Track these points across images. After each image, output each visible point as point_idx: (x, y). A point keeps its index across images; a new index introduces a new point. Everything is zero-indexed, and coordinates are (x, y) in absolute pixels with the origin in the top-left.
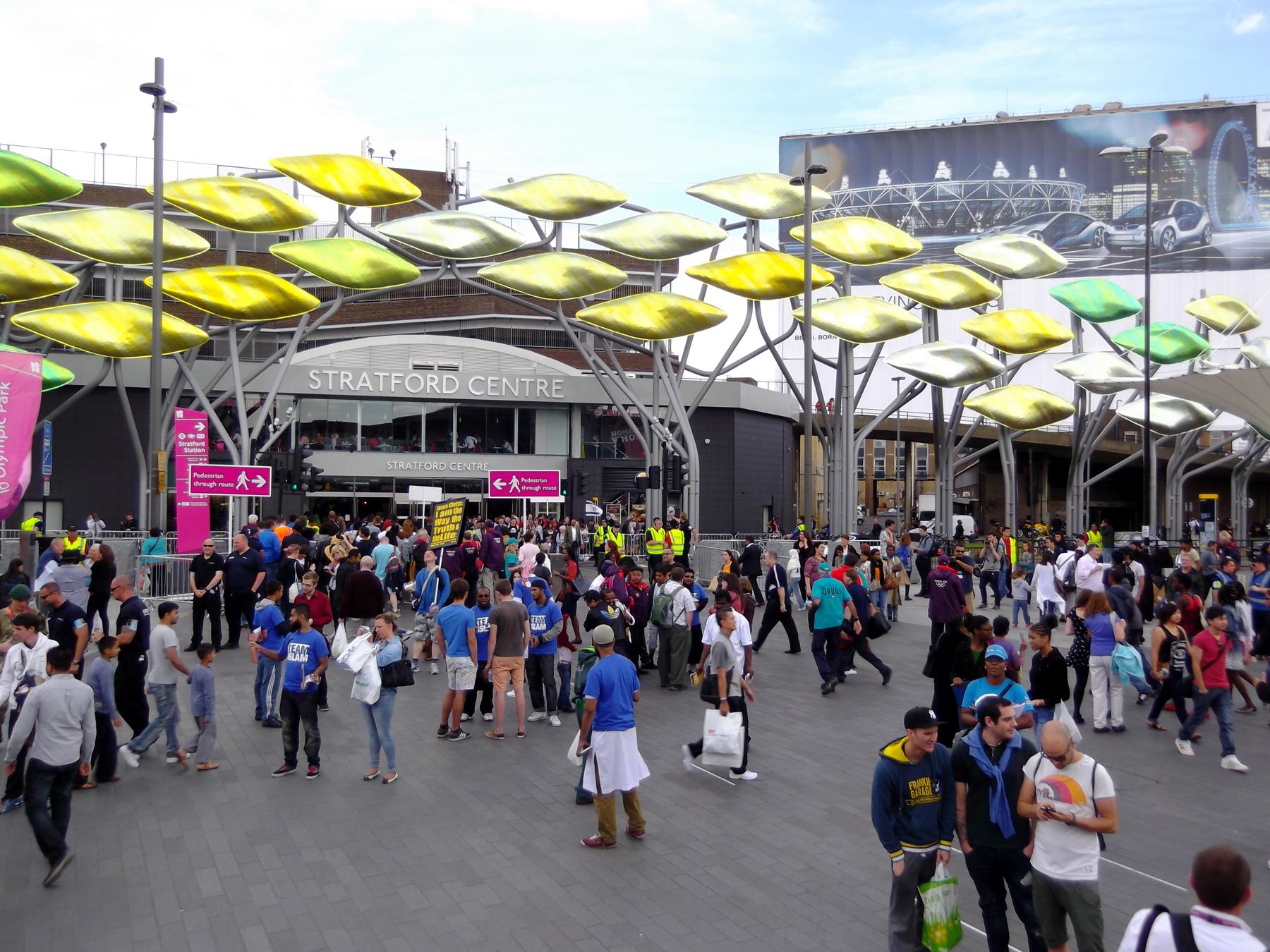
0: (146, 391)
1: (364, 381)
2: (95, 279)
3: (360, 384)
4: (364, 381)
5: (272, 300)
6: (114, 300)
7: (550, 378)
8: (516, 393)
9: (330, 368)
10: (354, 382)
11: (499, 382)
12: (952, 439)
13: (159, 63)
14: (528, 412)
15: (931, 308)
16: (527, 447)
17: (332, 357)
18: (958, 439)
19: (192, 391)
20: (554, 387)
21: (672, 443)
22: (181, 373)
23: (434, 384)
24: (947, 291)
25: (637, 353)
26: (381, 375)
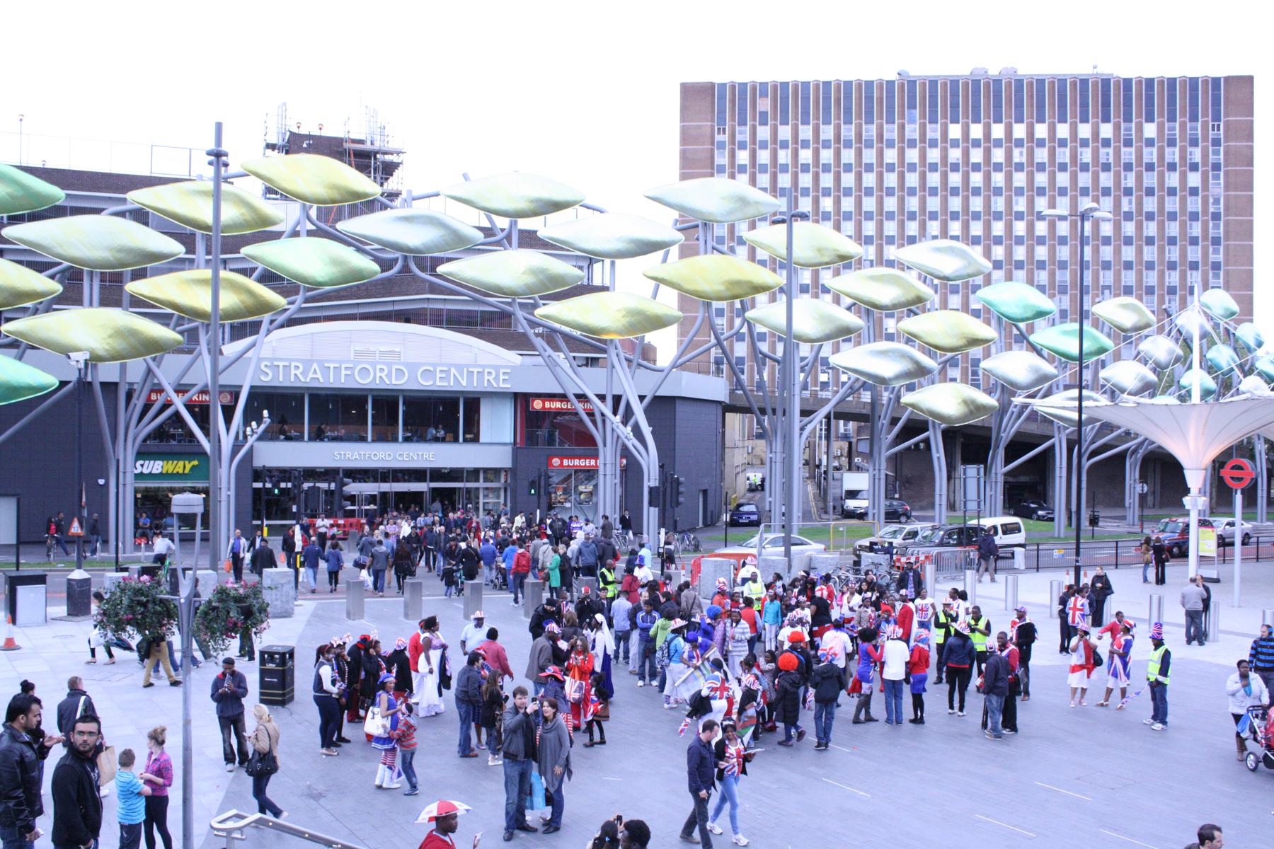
0: (116, 384)
1: (315, 372)
2: (74, 283)
3: (311, 375)
4: (315, 372)
5: (9, 194)
6: (91, 305)
7: (497, 368)
8: (464, 383)
9: (280, 360)
10: (304, 373)
11: (448, 372)
12: (885, 422)
13: (219, 127)
14: (473, 403)
15: (869, 309)
16: (473, 435)
17: (274, 344)
18: (894, 421)
19: (159, 384)
20: (502, 377)
21: (632, 442)
22: (149, 371)
23: (383, 375)
24: (886, 294)
25: (588, 347)
26: (332, 366)
